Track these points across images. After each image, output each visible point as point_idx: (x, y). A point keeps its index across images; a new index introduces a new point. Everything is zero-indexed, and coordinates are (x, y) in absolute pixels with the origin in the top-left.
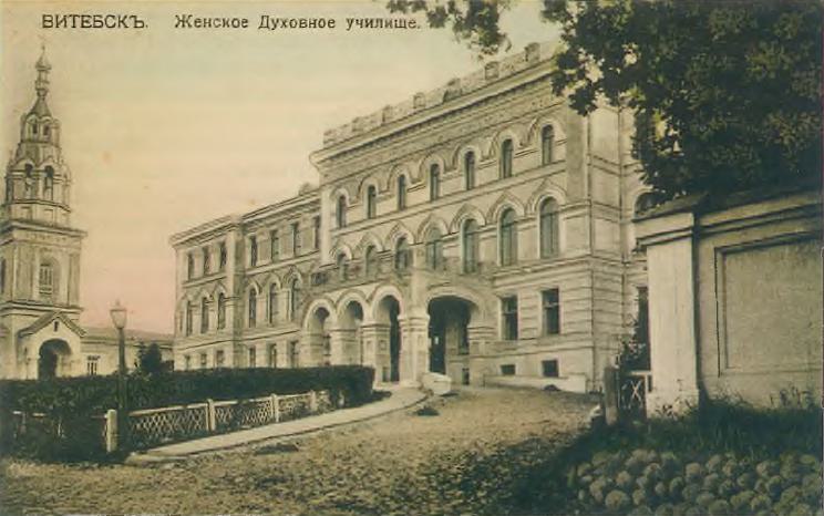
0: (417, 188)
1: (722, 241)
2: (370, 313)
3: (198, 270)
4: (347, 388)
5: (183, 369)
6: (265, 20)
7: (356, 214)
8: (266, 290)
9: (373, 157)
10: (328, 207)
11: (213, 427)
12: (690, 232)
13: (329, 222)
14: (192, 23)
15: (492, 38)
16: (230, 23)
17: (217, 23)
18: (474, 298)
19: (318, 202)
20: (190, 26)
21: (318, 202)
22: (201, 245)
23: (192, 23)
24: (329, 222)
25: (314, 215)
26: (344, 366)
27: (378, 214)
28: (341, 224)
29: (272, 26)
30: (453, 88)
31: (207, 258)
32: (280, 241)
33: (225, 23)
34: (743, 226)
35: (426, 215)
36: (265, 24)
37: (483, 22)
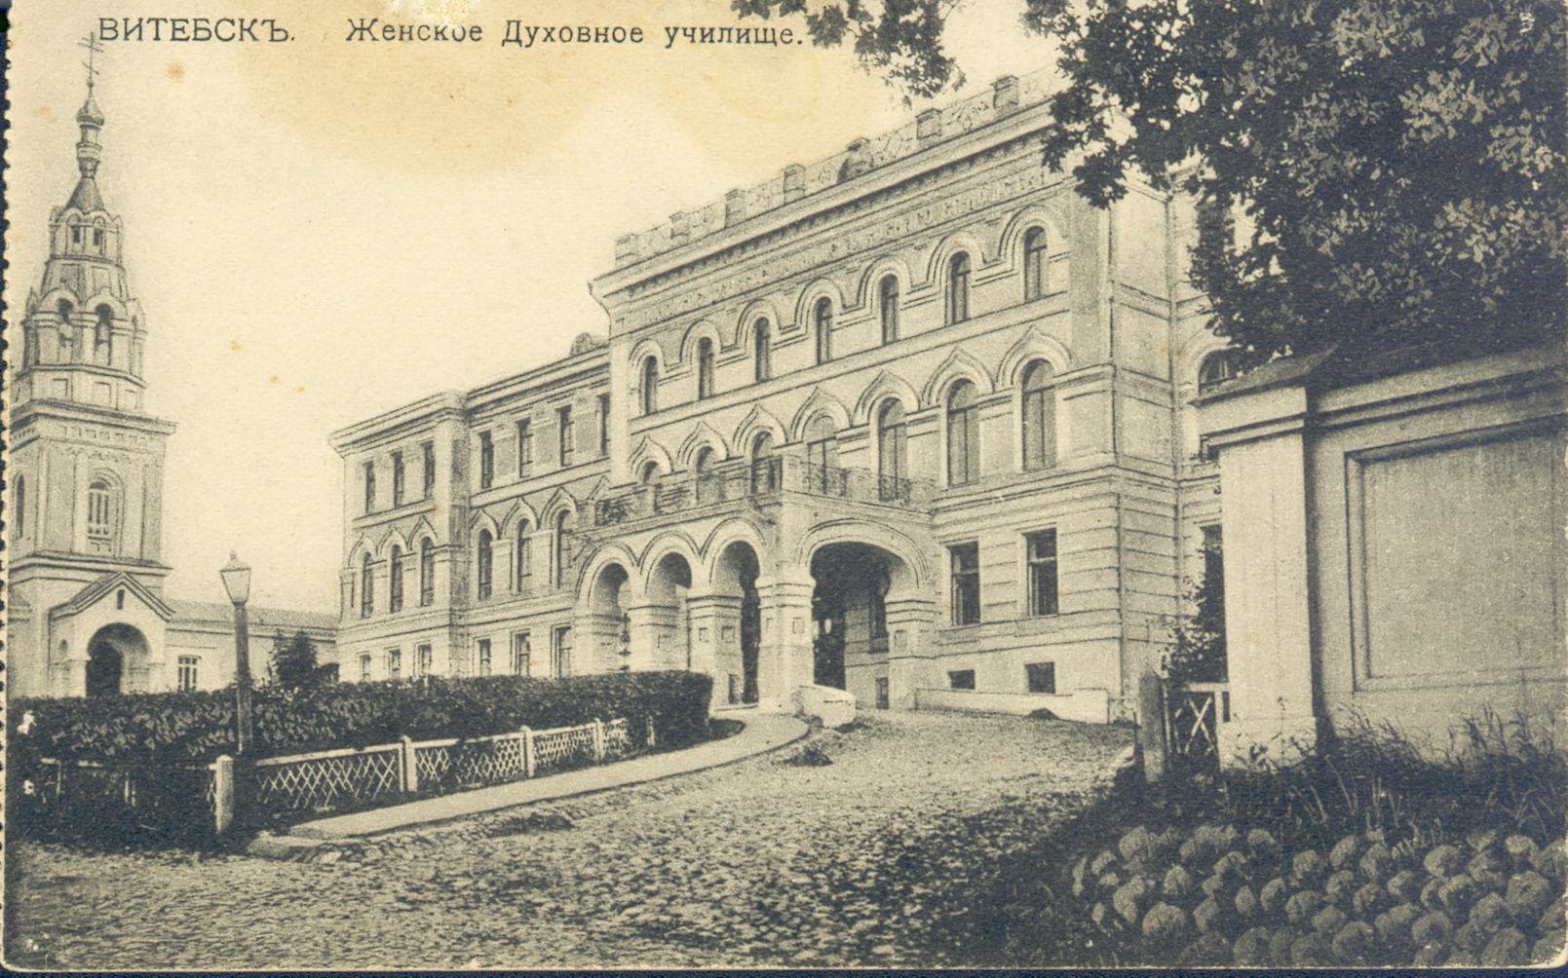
2: (705, 575)
3: (383, 498)
7: (671, 393)
13: (625, 404)
22: (387, 444)
23: (379, 35)
24: (625, 404)
25: (600, 391)
28: (649, 411)
29: (525, 39)
31: (399, 470)
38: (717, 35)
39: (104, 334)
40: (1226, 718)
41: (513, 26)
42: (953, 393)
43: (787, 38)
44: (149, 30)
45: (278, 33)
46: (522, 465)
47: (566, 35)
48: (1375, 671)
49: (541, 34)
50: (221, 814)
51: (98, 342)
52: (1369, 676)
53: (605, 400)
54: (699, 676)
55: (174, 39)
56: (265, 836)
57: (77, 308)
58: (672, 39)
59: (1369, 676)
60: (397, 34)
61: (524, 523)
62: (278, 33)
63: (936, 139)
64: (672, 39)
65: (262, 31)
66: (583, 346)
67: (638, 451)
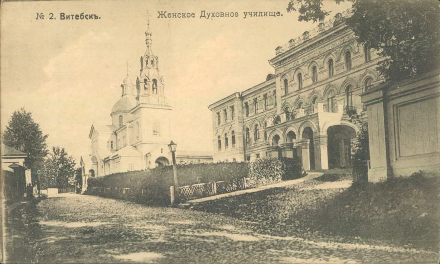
0: (322, 72)
1: (395, 102)
4: (40, 218)
5: (287, 152)
6: (203, 12)
8: (253, 128)
9: (317, 51)
10: (279, 83)
11: (215, 192)
12: (382, 99)
14: (167, 16)
15: (320, 15)
16: (186, 15)
17: (179, 16)
18: (296, 138)
19: (275, 83)
20: (165, 17)
21: (275, 83)
23: (167, 16)
24: (280, 93)
26: (328, 147)
27: (289, 93)
29: (207, 17)
30: (338, 20)
31: (226, 114)
32: (258, 104)
33: (184, 15)
34: (404, 94)
35: (297, 97)
36: (203, 15)
37: (312, 11)
38: (258, 14)
39: (155, 86)
40: (370, 168)
41: (203, 12)
42: (366, 82)
43: (278, 14)
44: (71, 17)
45: (96, 17)
46: (256, 110)
47: (232, 15)
48: (401, 155)
49: (211, 15)
50: (172, 199)
51: (153, 88)
52: (400, 156)
53: (275, 92)
54: (327, 134)
55: (202, 11)
56: (181, 204)
57: (148, 80)
58: (246, 16)
59: (400, 156)
60: (172, 16)
61: (257, 125)
62: (96, 17)
63: (308, 39)
64: (246, 16)
65: (93, 17)
66: (270, 77)
67: (284, 105)
